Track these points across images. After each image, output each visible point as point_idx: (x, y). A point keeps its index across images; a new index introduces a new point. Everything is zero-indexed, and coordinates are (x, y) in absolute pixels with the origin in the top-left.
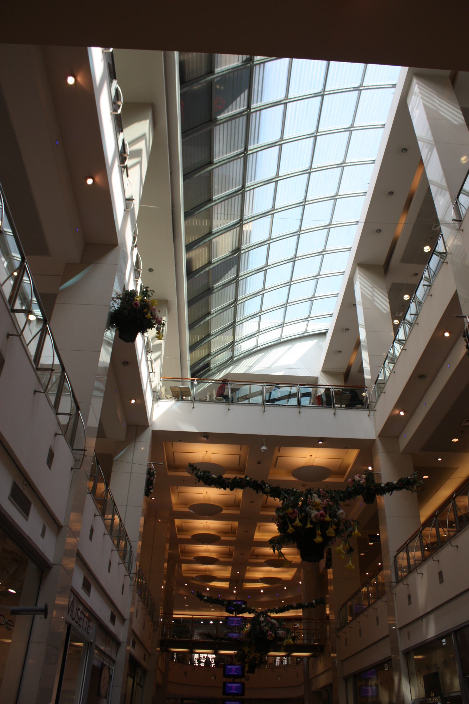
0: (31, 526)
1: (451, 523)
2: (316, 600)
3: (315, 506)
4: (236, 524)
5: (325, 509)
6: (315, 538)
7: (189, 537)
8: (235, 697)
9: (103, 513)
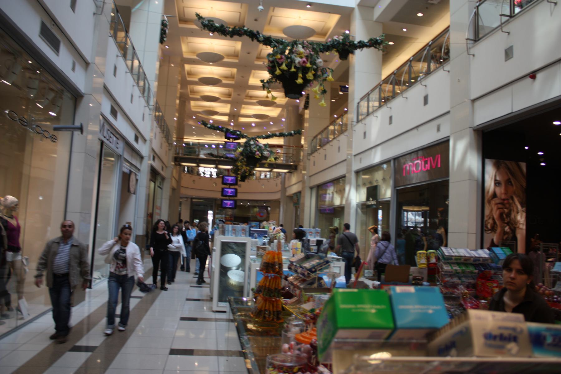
0: (62, 61)
1: (404, 83)
2: (294, 131)
3: (300, 54)
4: (235, 70)
5: (307, 57)
6: (297, 79)
7: (196, 80)
8: (231, 198)
9: (125, 56)
